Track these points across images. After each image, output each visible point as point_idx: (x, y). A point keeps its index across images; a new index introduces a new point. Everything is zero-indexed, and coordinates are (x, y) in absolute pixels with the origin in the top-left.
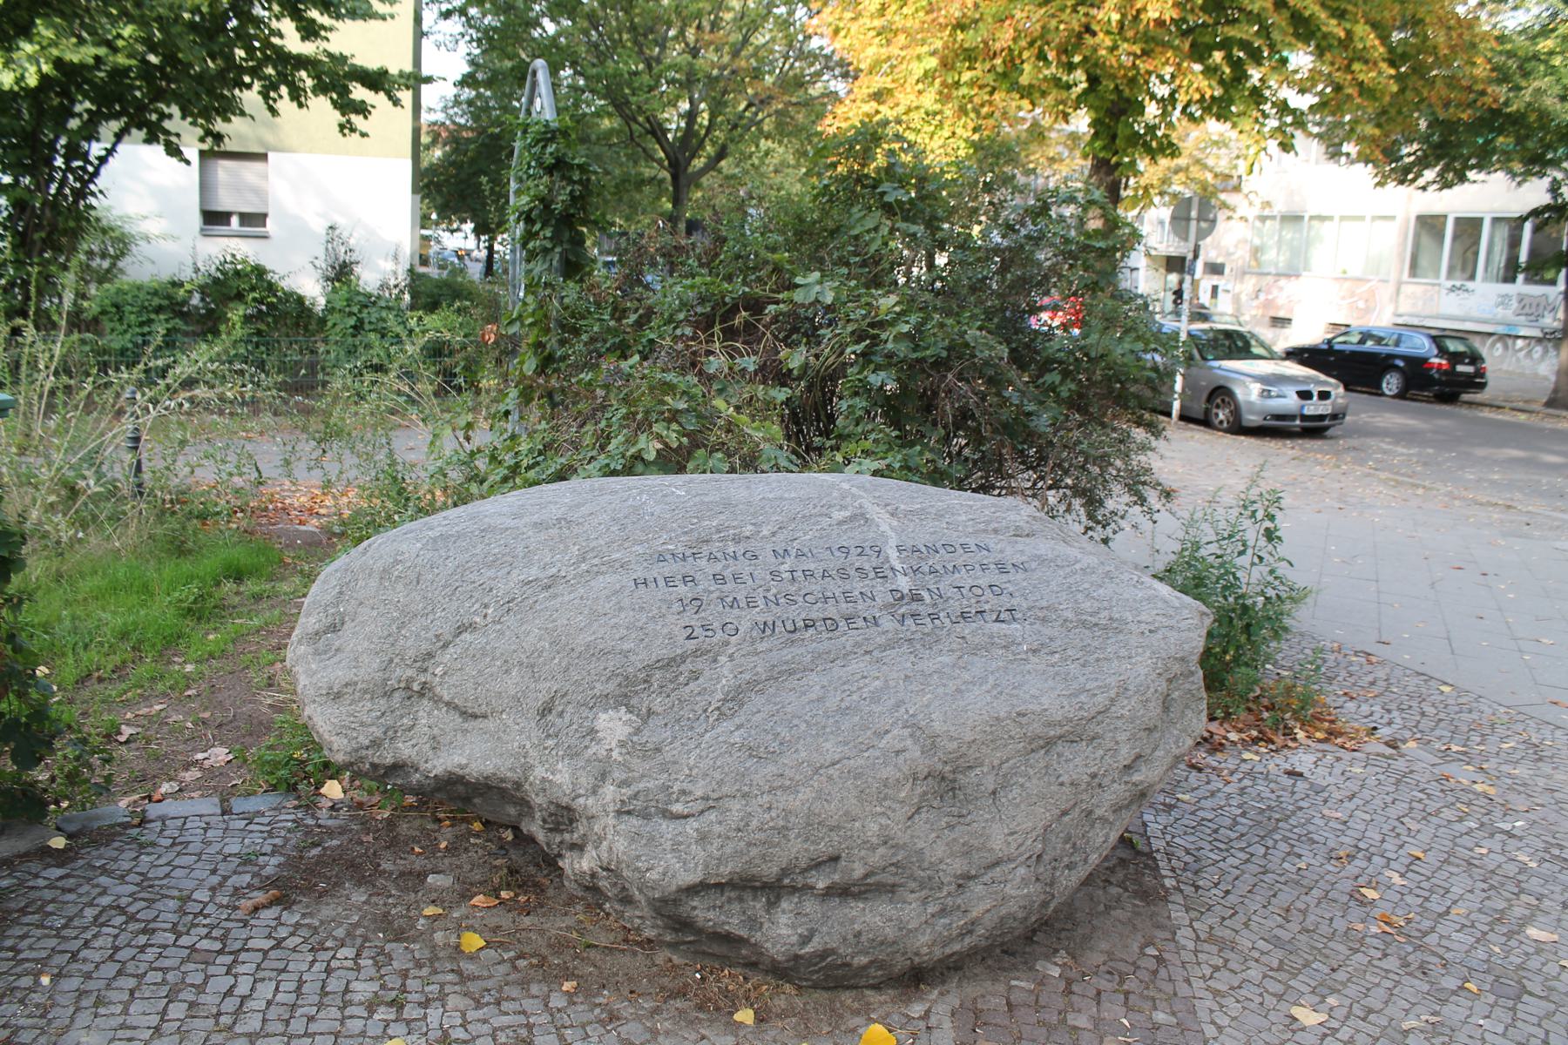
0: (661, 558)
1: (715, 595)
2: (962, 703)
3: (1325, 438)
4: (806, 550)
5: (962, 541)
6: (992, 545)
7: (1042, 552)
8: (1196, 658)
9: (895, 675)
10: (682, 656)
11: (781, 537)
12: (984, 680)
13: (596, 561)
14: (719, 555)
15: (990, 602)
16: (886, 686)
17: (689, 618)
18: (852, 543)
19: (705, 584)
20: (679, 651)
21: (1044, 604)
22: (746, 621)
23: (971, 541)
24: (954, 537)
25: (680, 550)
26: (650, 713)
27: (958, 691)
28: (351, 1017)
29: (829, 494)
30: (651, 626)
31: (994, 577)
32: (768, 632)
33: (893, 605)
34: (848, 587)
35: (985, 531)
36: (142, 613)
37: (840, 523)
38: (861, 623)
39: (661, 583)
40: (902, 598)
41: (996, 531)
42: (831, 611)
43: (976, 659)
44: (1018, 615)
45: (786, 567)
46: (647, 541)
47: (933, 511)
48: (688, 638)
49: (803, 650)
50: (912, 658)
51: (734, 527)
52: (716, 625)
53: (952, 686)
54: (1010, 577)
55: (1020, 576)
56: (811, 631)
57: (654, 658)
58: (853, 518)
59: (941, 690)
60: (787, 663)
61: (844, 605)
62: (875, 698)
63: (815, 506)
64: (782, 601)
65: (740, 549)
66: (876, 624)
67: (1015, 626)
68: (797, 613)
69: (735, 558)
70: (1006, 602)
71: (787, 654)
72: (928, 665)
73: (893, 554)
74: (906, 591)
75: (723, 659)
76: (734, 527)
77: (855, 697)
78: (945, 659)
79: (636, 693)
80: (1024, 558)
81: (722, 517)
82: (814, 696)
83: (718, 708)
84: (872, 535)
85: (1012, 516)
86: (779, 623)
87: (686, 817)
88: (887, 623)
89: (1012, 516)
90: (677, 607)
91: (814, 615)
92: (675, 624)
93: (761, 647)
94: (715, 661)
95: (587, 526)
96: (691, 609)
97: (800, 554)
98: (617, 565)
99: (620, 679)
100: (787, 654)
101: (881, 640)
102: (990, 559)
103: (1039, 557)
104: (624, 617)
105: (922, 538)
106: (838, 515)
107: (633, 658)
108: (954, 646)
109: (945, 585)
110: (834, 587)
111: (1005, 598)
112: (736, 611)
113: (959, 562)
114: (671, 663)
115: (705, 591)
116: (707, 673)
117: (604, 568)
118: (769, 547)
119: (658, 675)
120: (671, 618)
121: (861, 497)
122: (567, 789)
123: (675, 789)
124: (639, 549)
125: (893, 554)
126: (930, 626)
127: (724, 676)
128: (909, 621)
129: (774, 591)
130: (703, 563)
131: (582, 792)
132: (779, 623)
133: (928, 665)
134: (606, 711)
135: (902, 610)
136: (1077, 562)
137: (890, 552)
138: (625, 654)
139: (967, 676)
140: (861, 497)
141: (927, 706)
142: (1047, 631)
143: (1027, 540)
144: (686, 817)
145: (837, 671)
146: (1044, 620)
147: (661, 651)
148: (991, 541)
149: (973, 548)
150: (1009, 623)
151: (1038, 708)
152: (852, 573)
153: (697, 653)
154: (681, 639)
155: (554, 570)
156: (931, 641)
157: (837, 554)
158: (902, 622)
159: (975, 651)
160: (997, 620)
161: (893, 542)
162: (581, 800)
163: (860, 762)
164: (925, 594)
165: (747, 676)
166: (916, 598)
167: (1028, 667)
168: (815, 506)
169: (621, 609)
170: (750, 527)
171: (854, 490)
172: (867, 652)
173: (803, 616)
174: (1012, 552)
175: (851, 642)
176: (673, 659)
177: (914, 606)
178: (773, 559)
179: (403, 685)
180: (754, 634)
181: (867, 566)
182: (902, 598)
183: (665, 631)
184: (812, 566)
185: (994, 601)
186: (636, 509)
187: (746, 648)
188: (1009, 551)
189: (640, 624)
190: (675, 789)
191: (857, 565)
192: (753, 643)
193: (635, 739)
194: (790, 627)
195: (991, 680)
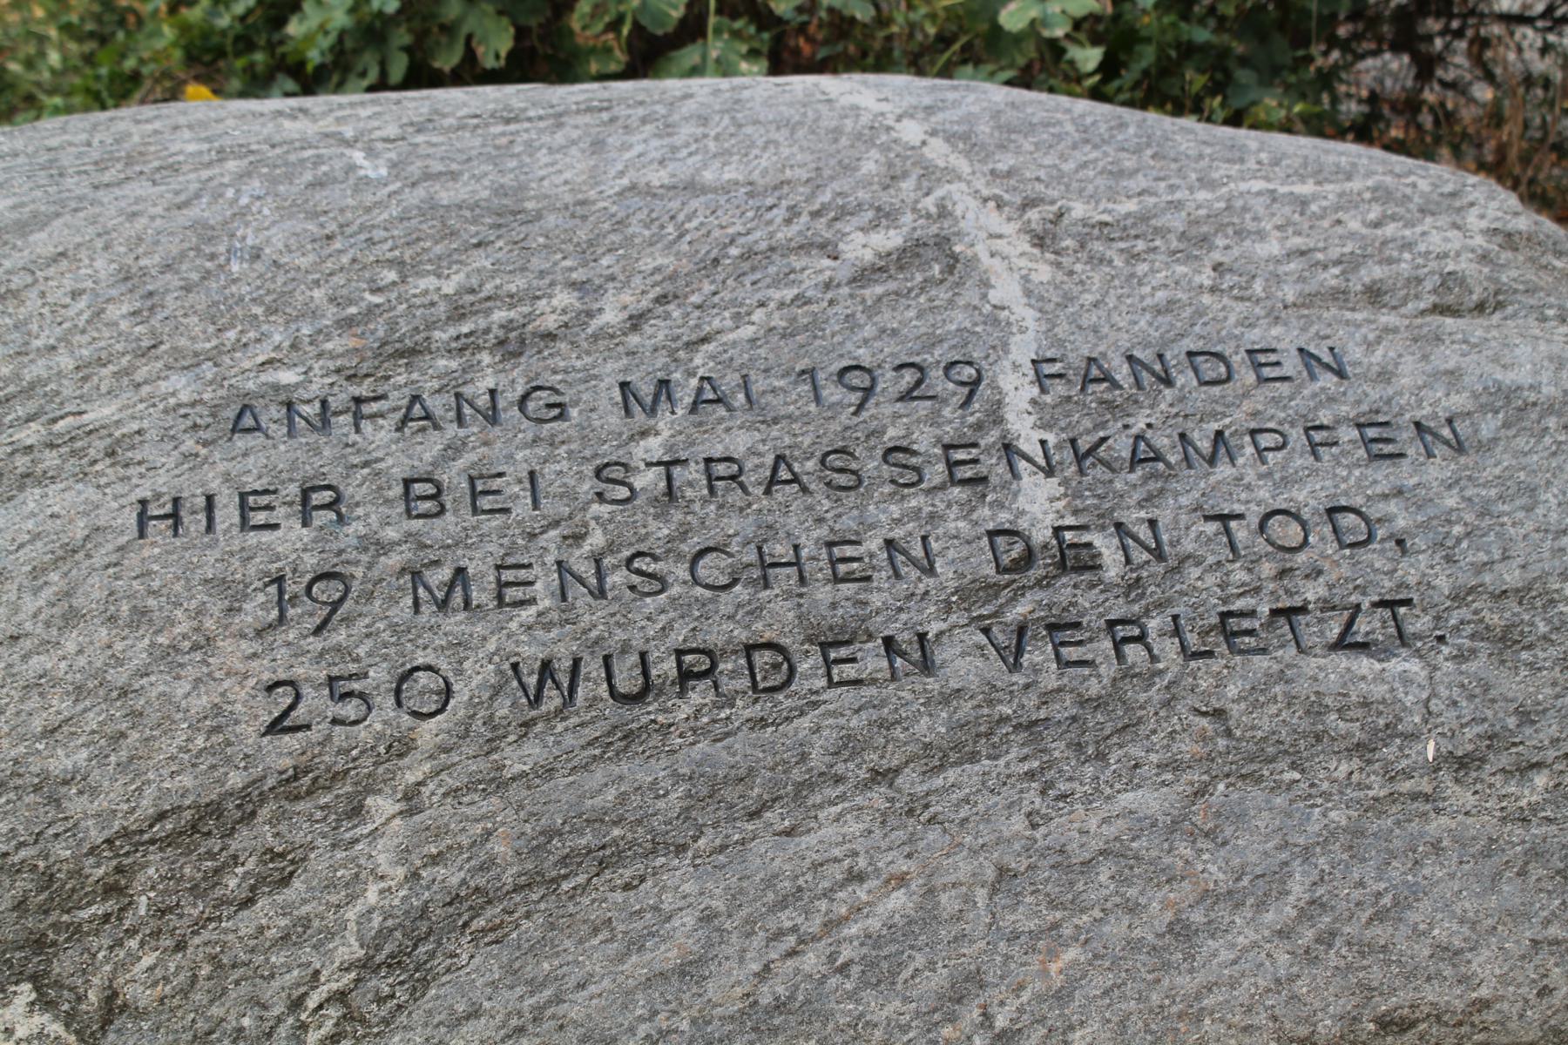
1: (394, 560)
2: (1186, 983)
4: (730, 381)
5: (1254, 337)
6: (1354, 353)
7: (1520, 376)
9: (963, 867)
10: (243, 795)
11: (656, 332)
12: (1273, 883)
13: (31, 434)
14: (438, 405)
15: (1327, 573)
16: (926, 916)
17: (299, 655)
18: (891, 350)
19: (374, 516)
20: (236, 780)
21: (1512, 577)
22: (479, 655)
23: (1286, 338)
24: (1231, 324)
26: (113, 1006)
27: (1180, 931)
29: (848, 168)
30: (157, 684)
31: (1346, 476)
32: (552, 699)
33: (993, 589)
34: (848, 523)
35: (1338, 296)
36: (1094, 319)
37: (863, 276)
38: (873, 661)
39: (228, 514)
40: (1028, 558)
41: (1374, 294)
42: (778, 617)
43: (1256, 794)
44: (1419, 623)
45: (654, 447)
46: (214, 357)
47: (1177, 222)
48: (276, 727)
49: (659, 769)
50: (1032, 798)
51: (513, 300)
52: (379, 675)
53: (1158, 907)
54: (1405, 474)
55: (1438, 470)
56: (699, 694)
57: (147, 806)
58: (906, 257)
59: (1116, 928)
60: (597, 820)
61: (823, 593)
62: (880, 968)
63: (793, 213)
64: (617, 578)
65: (514, 382)
66: (927, 666)
67: (1405, 664)
68: (655, 627)
69: (492, 416)
70: (1380, 569)
71: (602, 787)
72: (1083, 828)
73: (1016, 391)
74: (1041, 535)
75: (382, 806)
76: (513, 300)
77: (811, 960)
78: (1148, 800)
79: (76, 930)
80: (1458, 401)
81: (481, 260)
82: (667, 955)
83: (341, 997)
84: (959, 319)
85: (1436, 237)
86: (593, 667)
88: (964, 662)
89: (1436, 237)
90: (258, 608)
91: (714, 636)
92: (237, 677)
93: (519, 758)
94: (356, 811)
95: (32, 301)
96: (304, 615)
97: (708, 398)
98: (98, 445)
99: (24, 883)
100: (602, 787)
101: (931, 727)
102: (1340, 405)
103: (1508, 394)
104: (79, 650)
105: (1120, 328)
106: (862, 246)
107: (77, 805)
108: (1186, 747)
109: (1177, 515)
110: (801, 525)
111: (1376, 558)
112: (456, 623)
113: (1237, 419)
114: (206, 821)
115: (364, 543)
116: (319, 863)
117: (50, 459)
118: (611, 371)
120: (231, 652)
121: (953, 175)
124: (181, 386)
125: (1016, 391)
126: (1108, 670)
127: (377, 869)
128: (1038, 654)
129: (597, 539)
130: (379, 435)
132: (593, 667)
133: (1083, 828)
135: (1021, 609)
137: (1008, 381)
138: (51, 789)
139: (1215, 872)
140: (953, 175)
141: (1061, 997)
142: (1513, 685)
143: (1475, 328)
145: (768, 855)
146: (1507, 641)
147: (174, 782)
148: (1352, 334)
149: (1292, 365)
150: (1384, 653)
151: (1453, 998)
152: (871, 465)
153: (296, 784)
154: (249, 733)
156: (1102, 727)
157: (833, 394)
158: (1013, 657)
159: (1252, 762)
160: (1342, 644)
161: (1023, 349)
164: (1105, 545)
165: (452, 875)
166: (1074, 560)
167: (1437, 825)
168: (793, 213)
169: (71, 618)
170: (563, 298)
171: (937, 151)
172: (881, 776)
173: (677, 638)
174: (1410, 371)
175: (829, 736)
176: (214, 809)
177: (1065, 590)
178: (615, 419)
180: (503, 709)
181: (924, 441)
182: (1028, 558)
183: (201, 702)
184: (739, 442)
185: (1340, 567)
186: (206, 233)
187: (469, 764)
188: (1409, 373)
189: (118, 677)
191: (892, 434)
192: (492, 745)
194: (627, 681)
195: (1298, 888)
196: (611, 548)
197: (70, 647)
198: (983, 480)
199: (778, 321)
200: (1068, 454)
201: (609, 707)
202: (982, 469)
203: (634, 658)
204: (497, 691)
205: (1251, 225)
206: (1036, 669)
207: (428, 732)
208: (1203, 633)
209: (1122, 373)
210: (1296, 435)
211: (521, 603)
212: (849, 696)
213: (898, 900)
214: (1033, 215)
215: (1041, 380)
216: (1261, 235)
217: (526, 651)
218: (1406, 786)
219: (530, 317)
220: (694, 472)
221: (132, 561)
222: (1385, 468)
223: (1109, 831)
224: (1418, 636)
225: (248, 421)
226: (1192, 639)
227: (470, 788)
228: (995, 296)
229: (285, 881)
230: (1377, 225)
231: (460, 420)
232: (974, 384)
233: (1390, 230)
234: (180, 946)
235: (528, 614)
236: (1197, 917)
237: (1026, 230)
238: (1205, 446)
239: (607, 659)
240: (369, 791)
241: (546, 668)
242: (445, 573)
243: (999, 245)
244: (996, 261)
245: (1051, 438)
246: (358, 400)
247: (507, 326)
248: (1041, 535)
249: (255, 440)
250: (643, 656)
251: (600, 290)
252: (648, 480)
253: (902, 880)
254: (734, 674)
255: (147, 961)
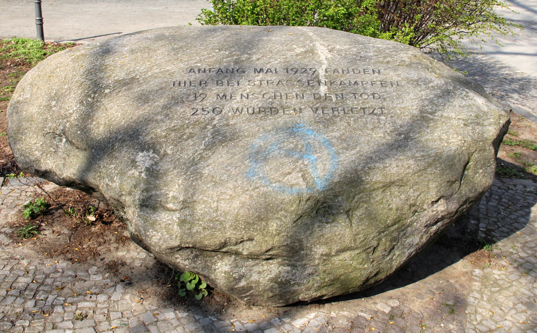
0: (191, 70)
3: (489, 328)
8: (490, 142)
25: (204, 66)
28: (387, 186)
32: (238, 113)
41: (388, 62)
44: (385, 111)
45: (259, 78)
64: (251, 97)
74: (323, 95)
87: (174, 211)
119: (173, 134)
122: (117, 190)
123: (170, 195)
128: (320, 111)
129: (248, 91)
131: (124, 193)
134: (142, 151)
136: (430, 82)
137: (320, 72)
144: (174, 211)
155: (134, 75)
161: (324, 67)
162: (123, 198)
163: (270, 189)
173: (260, 106)
179: (51, 131)
190: (170, 195)
193: (154, 167)
194: (251, 111)
196: (250, 92)
197: (162, 101)
198: (314, 86)
199: (282, 61)
200: (329, 83)
201: (247, 115)
202: (314, 84)
203: (252, 109)
204: (229, 112)
205: (368, 51)
206: (319, 114)
207: (217, 118)
208: (348, 111)
209: (340, 71)
210: (369, 82)
211: (235, 99)
212: (287, 116)
213: (292, 145)
214: (329, 47)
215: (326, 72)
216: (370, 52)
217: (234, 106)
218: (528, 190)
219: (239, 58)
220: (265, 82)
221: (172, 90)
222: (384, 88)
223: (328, 138)
224: (385, 113)
225: (192, 71)
226: (346, 111)
227: (224, 125)
228: (320, 59)
229: (193, 137)
230: (391, 52)
231: (227, 72)
232: (314, 72)
233: (393, 53)
234: (176, 145)
235: (235, 101)
236: (340, 151)
237: (328, 49)
238: (353, 83)
239: (247, 109)
240: (208, 125)
241: (237, 109)
242: (222, 94)
243: (323, 51)
244: (322, 54)
245: (327, 80)
246: (210, 69)
247: (236, 59)
248: (323, 95)
249: (193, 74)
250: (253, 108)
251: (253, 55)
252: (257, 83)
253: (293, 143)
254: (268, 112)
255: (171, 147)
